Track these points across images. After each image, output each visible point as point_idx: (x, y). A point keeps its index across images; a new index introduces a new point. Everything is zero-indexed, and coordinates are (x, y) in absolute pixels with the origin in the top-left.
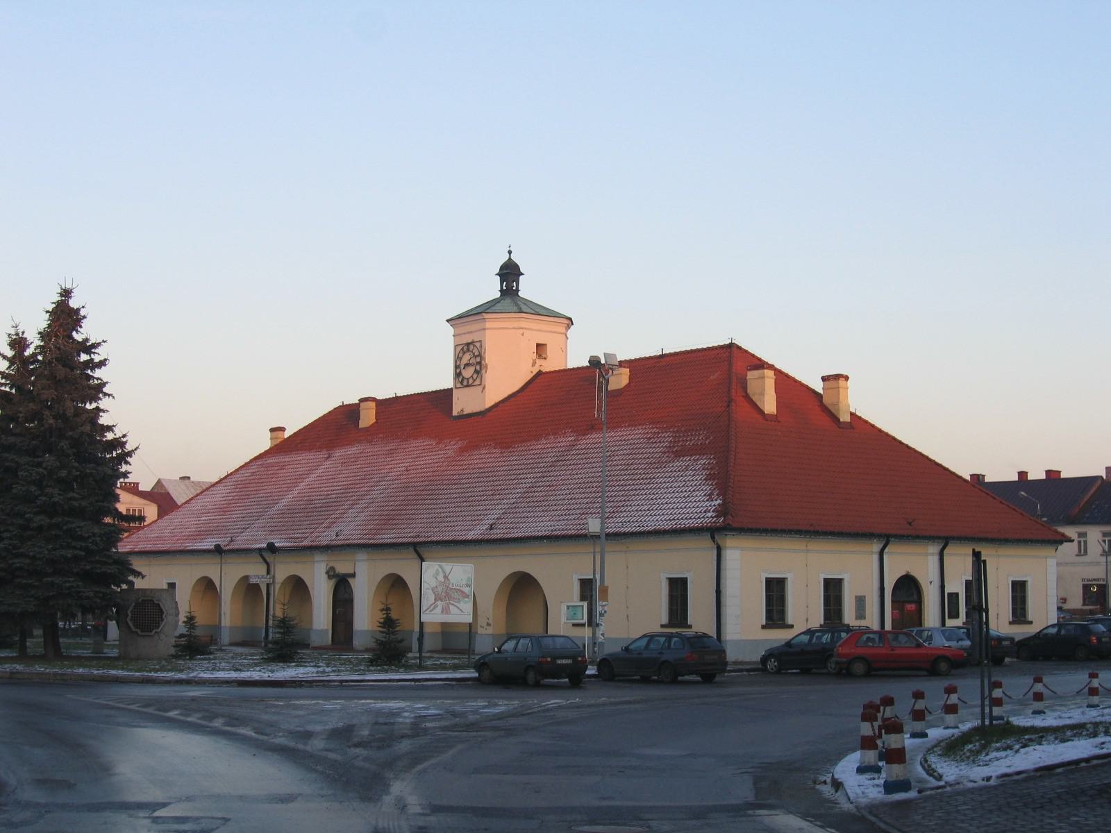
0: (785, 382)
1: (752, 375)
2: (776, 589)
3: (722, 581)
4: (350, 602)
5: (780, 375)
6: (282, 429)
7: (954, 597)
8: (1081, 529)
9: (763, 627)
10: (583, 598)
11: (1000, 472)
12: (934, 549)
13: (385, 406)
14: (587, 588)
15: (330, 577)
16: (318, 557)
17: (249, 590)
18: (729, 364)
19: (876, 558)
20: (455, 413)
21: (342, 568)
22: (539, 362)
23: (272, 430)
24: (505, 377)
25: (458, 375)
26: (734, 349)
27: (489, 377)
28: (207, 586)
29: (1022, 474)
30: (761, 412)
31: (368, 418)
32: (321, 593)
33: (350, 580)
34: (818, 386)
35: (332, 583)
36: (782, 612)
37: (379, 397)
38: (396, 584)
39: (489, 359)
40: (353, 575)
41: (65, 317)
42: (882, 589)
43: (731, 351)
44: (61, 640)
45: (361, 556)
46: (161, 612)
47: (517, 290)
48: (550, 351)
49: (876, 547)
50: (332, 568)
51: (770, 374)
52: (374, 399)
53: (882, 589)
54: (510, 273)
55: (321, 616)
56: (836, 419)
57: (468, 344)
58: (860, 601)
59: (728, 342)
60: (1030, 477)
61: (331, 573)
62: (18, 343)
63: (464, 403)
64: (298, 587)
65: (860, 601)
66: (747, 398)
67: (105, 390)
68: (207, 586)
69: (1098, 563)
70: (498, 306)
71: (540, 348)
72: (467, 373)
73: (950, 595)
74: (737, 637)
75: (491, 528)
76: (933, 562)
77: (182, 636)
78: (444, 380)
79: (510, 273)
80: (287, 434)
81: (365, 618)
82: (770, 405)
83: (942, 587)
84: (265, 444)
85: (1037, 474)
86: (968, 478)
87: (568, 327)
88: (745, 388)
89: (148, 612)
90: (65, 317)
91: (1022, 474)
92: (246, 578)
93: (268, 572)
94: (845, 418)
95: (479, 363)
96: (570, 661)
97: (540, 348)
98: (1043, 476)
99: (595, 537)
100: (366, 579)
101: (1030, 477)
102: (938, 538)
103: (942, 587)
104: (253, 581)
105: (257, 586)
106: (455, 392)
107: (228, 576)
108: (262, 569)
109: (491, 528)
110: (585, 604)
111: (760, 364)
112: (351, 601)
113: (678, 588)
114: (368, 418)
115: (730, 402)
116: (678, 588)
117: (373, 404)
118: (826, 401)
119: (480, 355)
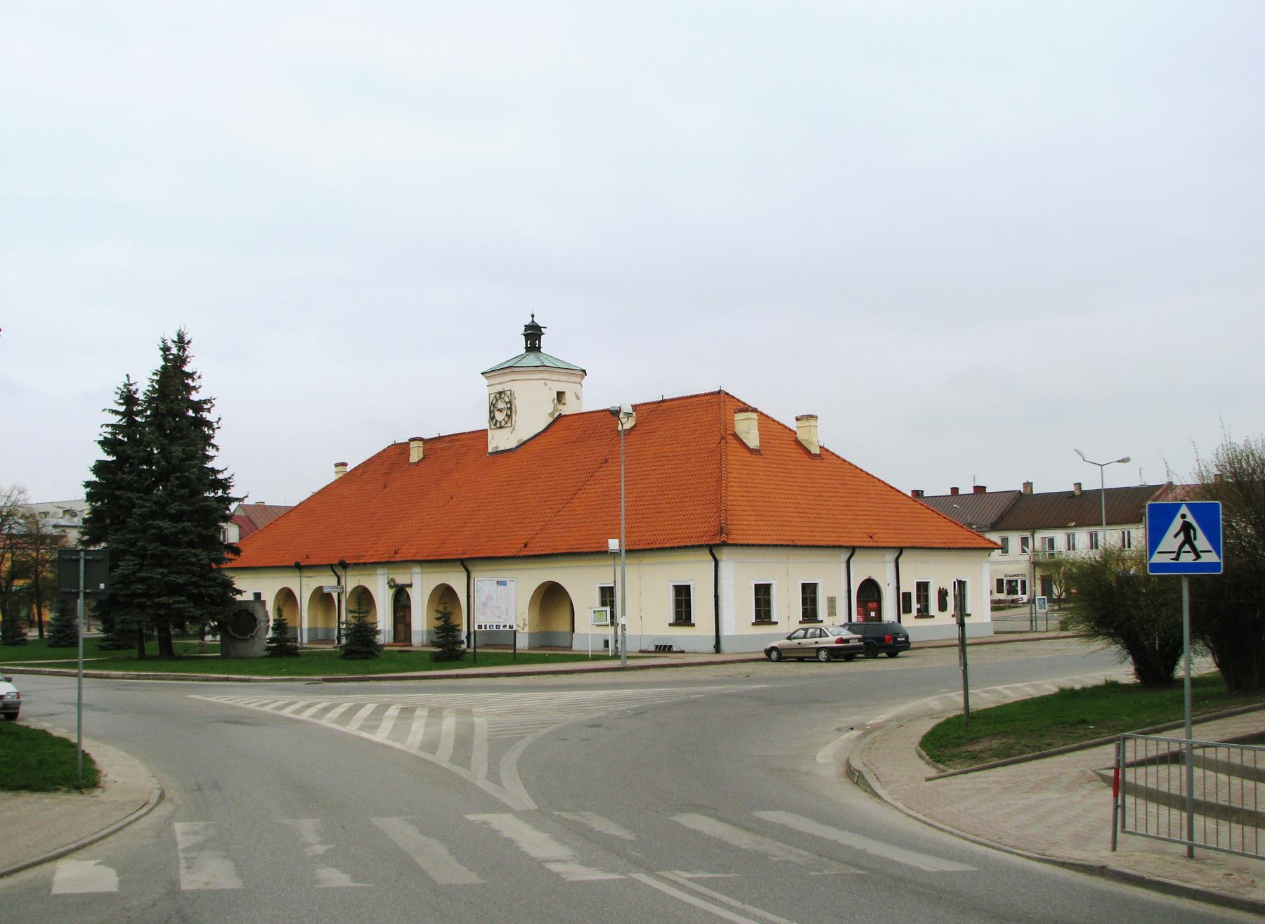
1: (739, 416)
2: (763, 593)
4: (408, 607)
6: (344, 464)
7: (907, 596)
8: (1004, 534)
10: (603, 604)
11: (936, 487)
12: (890, 557)
13: (431, 445)
14: (607, 595)
15: (391, 587)
16: (380, 571)
17: (322, 599)
18: (719, 405)
19: (844, 566)
20: (490, 450)
21: (401, 579)
22: (560, 407)
23: (337, 465)
24: (532, 418)
25: (492, 418)
28: (287, 597)
29: (955, 490)
31: (416, 455)
34: (793, 425)
35: (392, 592)
36: (768, 614)
37: (426, 437)
38: (445, 594)
39: (519, 404)
40: (411, 586)
41: (174, 375)
44: (173, 642)
45: (417, 569)
48: (568, 397)
49: (844, 556)
50: (393, 580)
54: (533, 334)
55: (383, 619)
56: (807, 451)
57: (500, 393)
58: (832, 602)
61: (392, 584)
62: (129, 398)
63: (500, 440)
64: (364, 597)
65: (832, 602)
66: (735, 436)
67: (213, 441)
68: (287, 597)
69: (1017, 562)
71: (560, 395)
72: (500, 416)
74: (733, 633)
77: (272, 640)
78: (482, 423)
79: (533, 334)
80: (349, 469)
81: (421, 621)
82: (753, 440)
83: (898, 588)
84: (331, 476)
86: (910, 494)
89: (241, 620)
90: (174, 375)
91: (955, 490)
92: (320, 589)
93: (339, 583)
94: (815, 450)
95: (510, 408)
97: (560, 395)
99: (615, 554)
100: (421, 586)
103: (898, 588)
104: (326, 591)
107: (304, 587)
108: (334, 581)
110: (608, 609)
111: (746, 409)
112: (409, 607)
113: (683, 594)
114: (416, 455)
116: (683, 594)
118: (800, 436)
119: (510, 402)
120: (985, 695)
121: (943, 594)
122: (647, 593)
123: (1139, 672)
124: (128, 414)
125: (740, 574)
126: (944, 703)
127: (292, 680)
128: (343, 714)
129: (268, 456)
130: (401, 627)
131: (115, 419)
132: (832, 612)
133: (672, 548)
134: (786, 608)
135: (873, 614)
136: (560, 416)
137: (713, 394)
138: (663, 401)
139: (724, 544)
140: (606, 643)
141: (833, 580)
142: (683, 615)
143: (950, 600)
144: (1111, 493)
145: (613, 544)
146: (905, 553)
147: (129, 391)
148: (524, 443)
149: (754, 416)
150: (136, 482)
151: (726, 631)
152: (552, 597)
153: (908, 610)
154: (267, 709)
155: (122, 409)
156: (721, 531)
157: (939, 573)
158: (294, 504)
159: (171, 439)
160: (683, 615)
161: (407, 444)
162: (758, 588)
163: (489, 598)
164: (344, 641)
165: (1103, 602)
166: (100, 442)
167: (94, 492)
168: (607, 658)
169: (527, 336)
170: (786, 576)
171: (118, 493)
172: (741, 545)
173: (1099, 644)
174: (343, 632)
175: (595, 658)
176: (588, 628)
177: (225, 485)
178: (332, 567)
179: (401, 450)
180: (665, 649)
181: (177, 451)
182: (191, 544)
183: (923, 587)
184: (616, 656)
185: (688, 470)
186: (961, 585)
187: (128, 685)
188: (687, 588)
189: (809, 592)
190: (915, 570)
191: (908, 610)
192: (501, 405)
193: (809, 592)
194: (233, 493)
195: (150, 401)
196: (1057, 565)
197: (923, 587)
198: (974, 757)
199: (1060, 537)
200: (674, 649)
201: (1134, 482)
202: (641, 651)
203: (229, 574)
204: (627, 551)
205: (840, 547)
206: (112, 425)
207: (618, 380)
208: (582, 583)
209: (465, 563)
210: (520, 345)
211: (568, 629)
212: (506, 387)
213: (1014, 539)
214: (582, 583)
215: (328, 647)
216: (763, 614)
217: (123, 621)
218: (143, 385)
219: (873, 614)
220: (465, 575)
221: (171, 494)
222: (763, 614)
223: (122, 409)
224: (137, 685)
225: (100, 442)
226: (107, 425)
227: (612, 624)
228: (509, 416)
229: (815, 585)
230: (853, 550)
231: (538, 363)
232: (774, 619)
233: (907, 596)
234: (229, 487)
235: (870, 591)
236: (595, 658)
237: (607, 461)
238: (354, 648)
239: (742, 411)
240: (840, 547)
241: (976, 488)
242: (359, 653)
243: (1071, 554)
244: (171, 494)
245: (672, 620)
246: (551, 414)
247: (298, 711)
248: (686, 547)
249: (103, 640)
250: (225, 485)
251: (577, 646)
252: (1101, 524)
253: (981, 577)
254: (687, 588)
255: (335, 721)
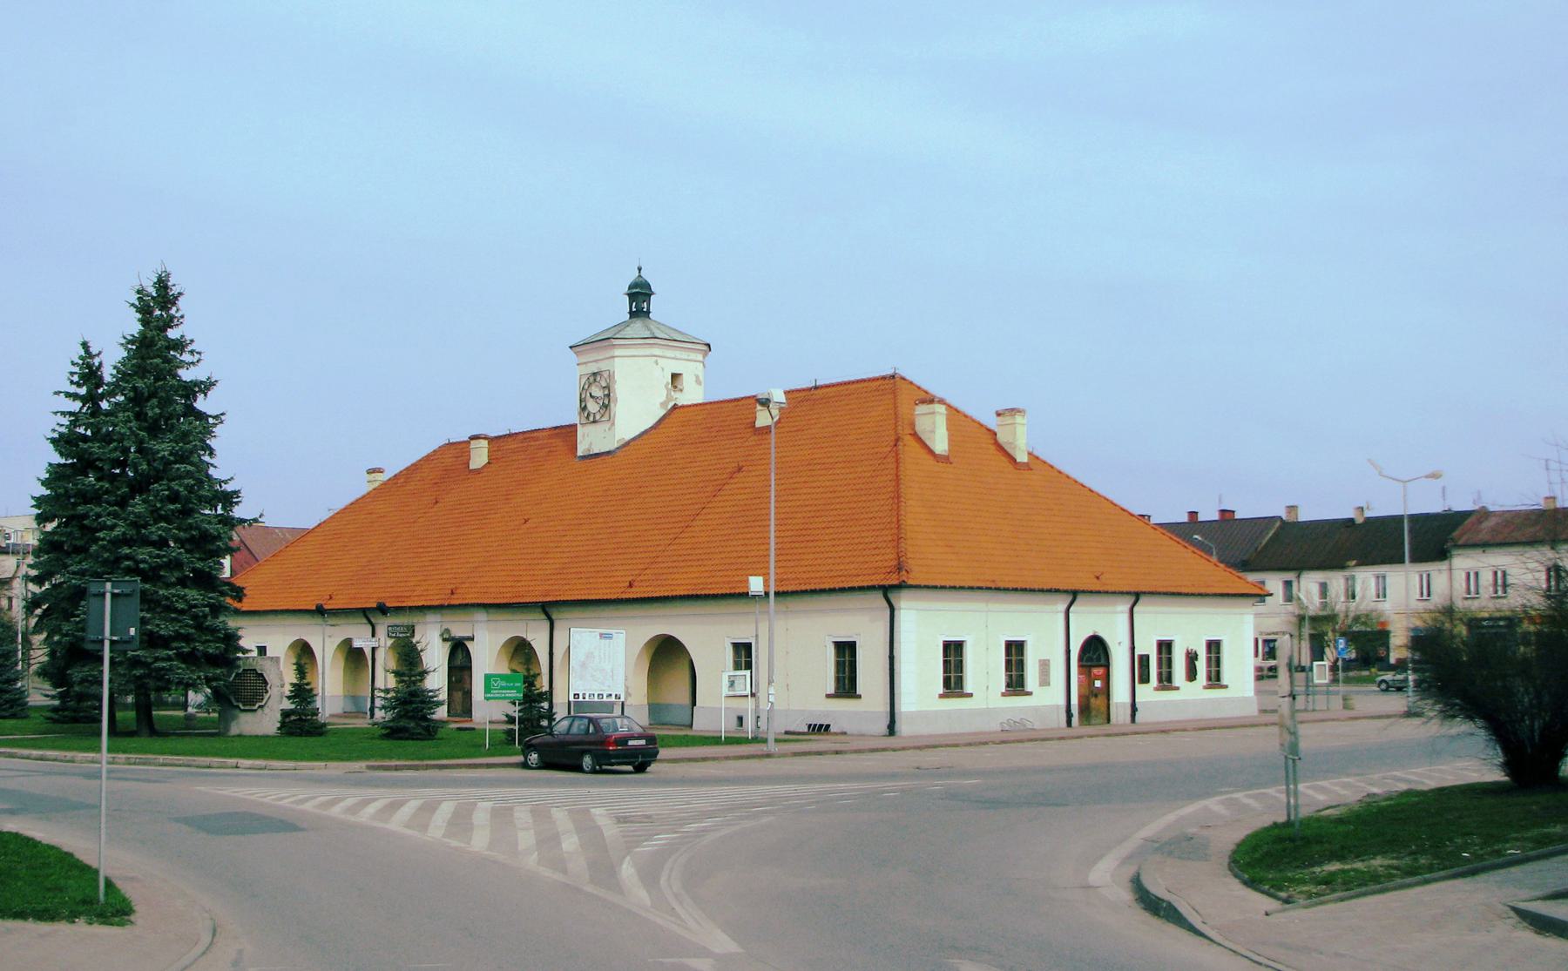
0: (956, 416)
1: (921, 409)
2: (953, 651)
3: (271, 617)
5: (953, 412)
6: (380, 471)
7: (1145, 659)
9: (1003, 695)
12: (1123, 607)
13: (802, 399)
14: (743, 654)
16: (431, 617)
18: (891, 392)
19: (1062, 617)
20: (580, 453)
21: (459, 631)
24: (637, 409)
26: (899, 383)
27: (620, 409)
30: (931, 452)
31: (479, 457)
32: (435, 657)
33: (469, 644)
34: (991, 422)
35: (448, 644)
38: (520, 650)
39: (621, 390)
41: (156, 347)
42: (1068, 652)
43: (891, 384)
45: (481, 616)
46: (266, 682)
47: (648, 312)
48: (687, 381)
50: (447, 630)
51: (941, 409)
52: (486, 438)
53: (1068, 652)
54: (640, 295)
56: (1012, 459)
57: (594, 374)
58: (1045, 666)
59: (891, 372)
60: (1201, 518)
62: (89, 374)
63: (591, 440)
65: (1045, 666)
66: (915, 435)
70: (629, 332)
72: (593, 407)
73: (1141, 657)
74: (913, 709)
75: (631, 586)
76: (1124, 619)
78: (571, 416)
79: (640, 295)
80: (383, 477)
82: (940, 444)
83: (1133, 649)
85: (1209, 514)
87: (705, 354)
88: (912, 425)
90: (156, 347)
91: (1193, 514)
96: (643, 742)
98: (1216, 517)
101: (1201, 518)
102: (1128, 593)
103: (1133, 649)
105: (360, 651)
106: (580, 430)
107: (325, 641)
109: (631, 586)
111: (930, 400)
112: (470, 668)
113: (846, 651)
114: (479, 457)
115: (897, 440)
116: (846, 651)
117: (485, 443)
118: (1001, 438)
119: (608, 387)
120: (1310, 792)
121: (1191, 658)
122: (798, 647)
123: (1509, 766)
124: (91, 399)
125: (923, 626)
126: (1262, 808)
127: (416, 768)
128: (382, 811)
129: (283, 458)
130: (458, 695)
131: (76, 406)
132: (1045, 681)
133: (832, 591)
134: (986, 669)
135: (1098, 684)
136: (675, 407)
137: (884, 378)
138: (816, 388)
139: (901, 586)
140: (740, 719)
141: (1046, 632)
142: (846, 685)
143: (1201, 665)
144: (1414, 518)
145: (756, 584)
146: (1143, 599)
147: (89, 366)
148: (628, 443)
149: (941, 409)
150: (107, 492)
151: (906, 705)
152: (666, 652)
153: (1145, 679)
154: (308, 806)
155: (83, 391)
156: (899, 568)
157: (1187, 627)
158: (310, 523)
159: (154, 429)
160: (846, 685)
161: (468, 443)
162: (1009, 645)
163: (590, 655)
164: (379, 714)
165: (1457, 669)
166: (53, 441)
167: (46, 509)
168: (745, 741)
169: (633, 297)
170: (985, 628)
171: (81, 509)
172: (1187, 595)
173: (1461, 726)
174: (378, 703)
175: (731, 741)
176: (719, 693)
177: (229, 499)
178: (365, 612)
179: (459, 450)
180: (821, 729)
181: (163, 448)
182: (183, 582)
183: (1165, 647)
184: (755, 740)
185: (845, 486)
186: (1214, 647)
187: (192, 774)
188: (748, 646)
189: (1015, 650)
190: (1160, 623)
191: (1145, 679)
192: (597, 392)
193: (1015, 650)
194: (238, 512)
195: (123, 375)
196: (1331, 618)
197: (1165, 647)
198: (1328, 881)
199: (1336, 581)
200: (832, 729)
201: (1435, 507)
202: (787, 733)
203: (232, 623)
204: (777, 594)
205: (1057, 591)
206: (71, 414)
207: (768, 360)
208: (707, 638)
209: (547, 609)
210: (621, 307)
211: (687, 700)
212: (603, 366)
213: (1274, 583)
214: (707, 638)
215: (363, 723)
216: (953, 683)
217: (83, 681)
218: (111, 358)
219: (1098, 684)
220: (547, 624)
221: (155, 511)
222: (953, 683)
223: (83, 391)
224: (206, 774)
225: (53, 441)
226: (63, 413)
227: (753, 695)
228: (606, 407)
229: (854, 644)
230: (1075, 594)
231: (647, 334)
232: (968, 688)
233: (1145, 659)
234: (232, 504)
235: (1095, 651)
236: (731, 741)
237: (740, 469)
238: (402, 723)
239: (923, 402)
240: (1057, 591)
241: (1223, 512)
242: (410, 726)
243: (1475, 605)
244: (155, 511)
245: (831, 689)
246: (663, 405)
247: (353, 810)
248: (1200, 595)
249: (55, 709)
250: (229, 499)
251: (701, 724)
252: (1402, 561)
253: (1237, 630)
254: (748, 646)
255: (407, 826)
